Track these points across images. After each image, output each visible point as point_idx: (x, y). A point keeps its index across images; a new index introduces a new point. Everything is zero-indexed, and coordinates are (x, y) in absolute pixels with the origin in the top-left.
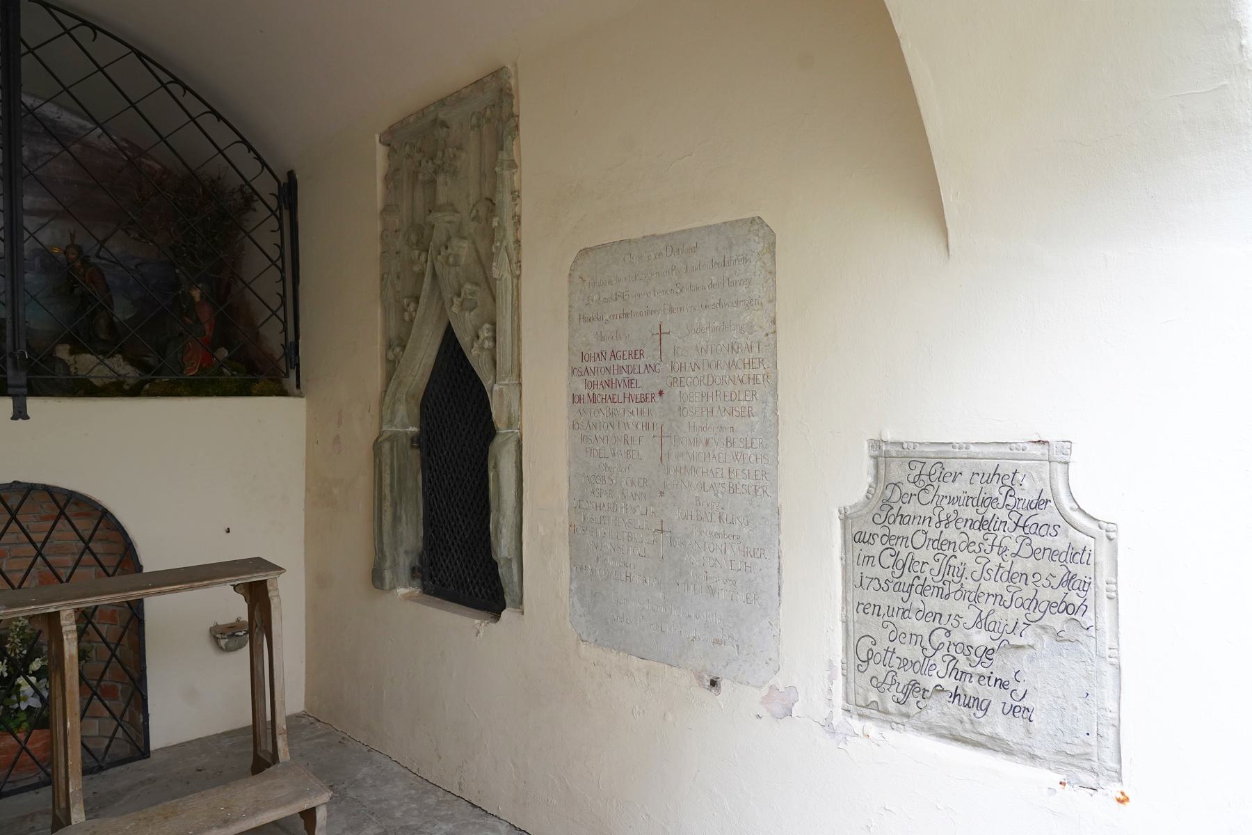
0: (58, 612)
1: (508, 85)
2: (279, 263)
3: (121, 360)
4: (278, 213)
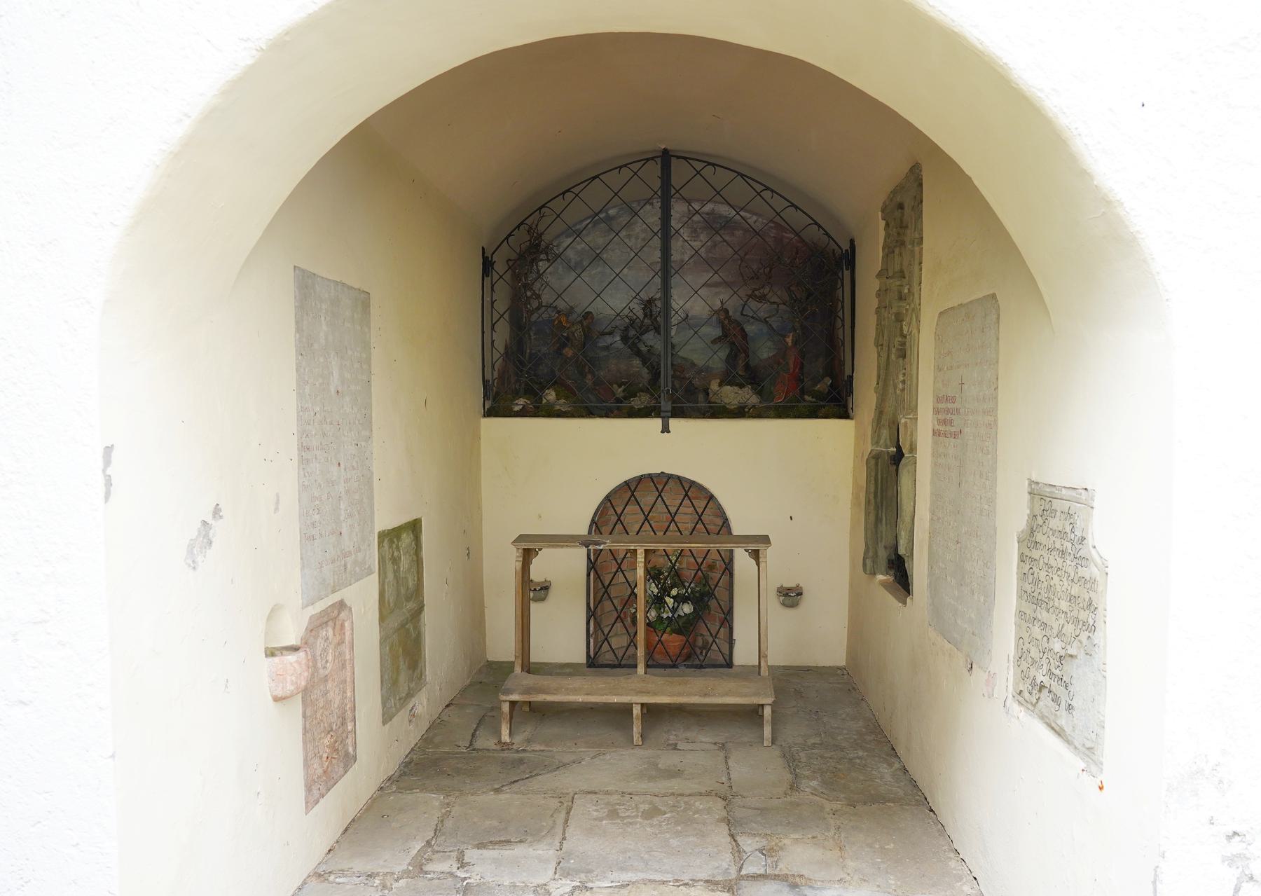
0: (636, 550)
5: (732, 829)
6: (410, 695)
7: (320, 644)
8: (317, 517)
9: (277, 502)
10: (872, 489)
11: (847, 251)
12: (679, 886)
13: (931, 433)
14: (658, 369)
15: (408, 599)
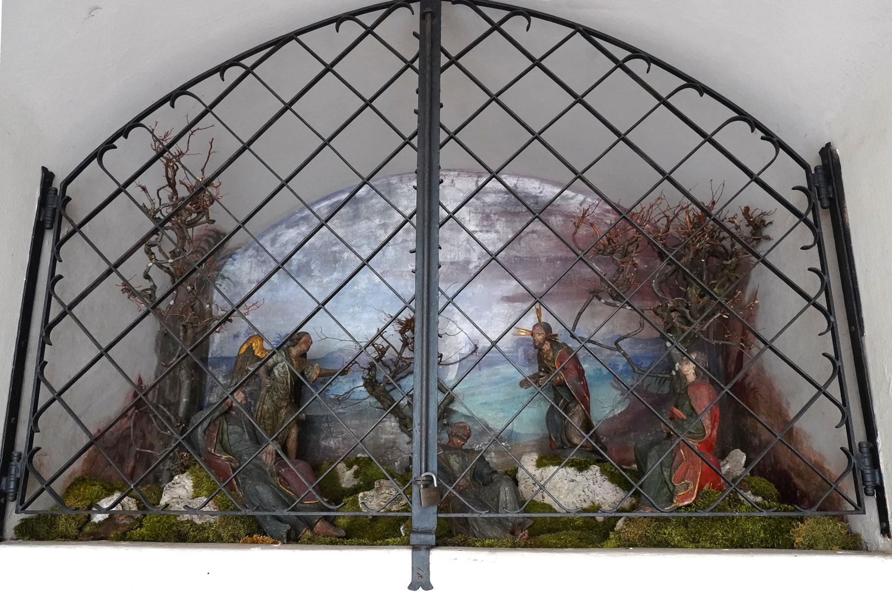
2: (822, 301)
3: (598, 474)
4: (810, 217)
14: (623, 510)
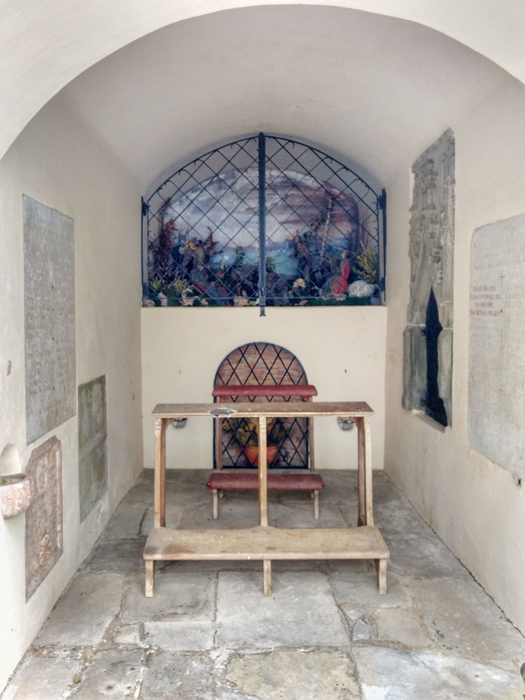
1: (452, 138)
5: (337, 599)
6: (98, 499)
7: (39, 470)
8: (37, 377)
9: (10, 367)
10: (408, 351)
11: (380, 197)
12: (309, 652)
13: (468, 313)
15: (97, 431)
